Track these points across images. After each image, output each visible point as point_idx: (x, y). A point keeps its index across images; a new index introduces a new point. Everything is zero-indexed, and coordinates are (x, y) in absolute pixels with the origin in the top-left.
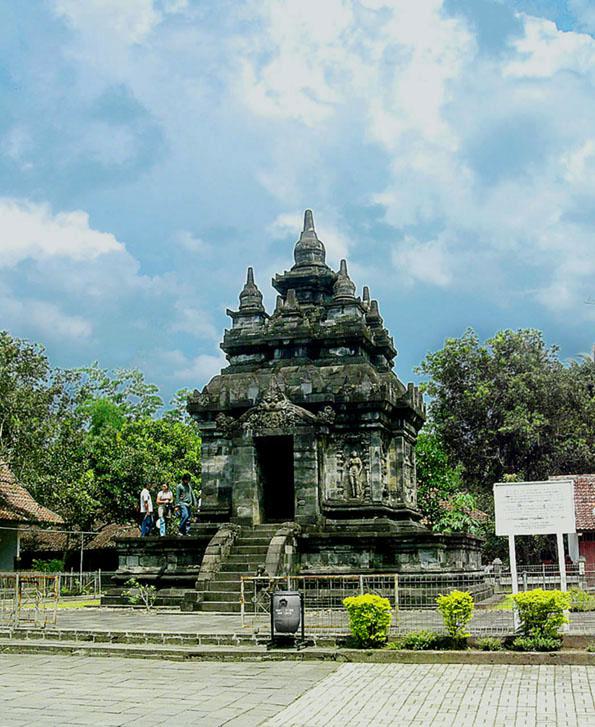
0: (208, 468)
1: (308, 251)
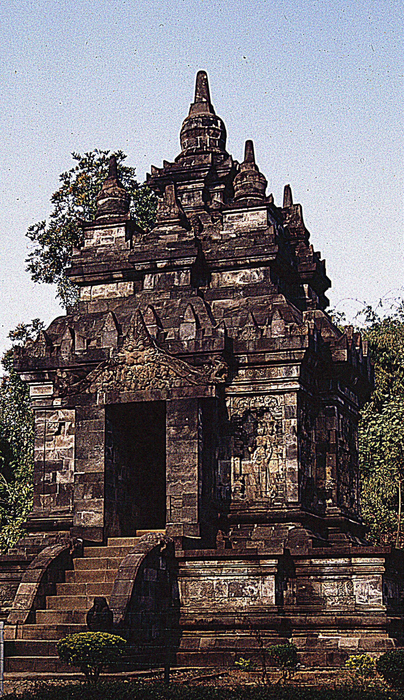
0: (45, 454)
1: (204, 127)
